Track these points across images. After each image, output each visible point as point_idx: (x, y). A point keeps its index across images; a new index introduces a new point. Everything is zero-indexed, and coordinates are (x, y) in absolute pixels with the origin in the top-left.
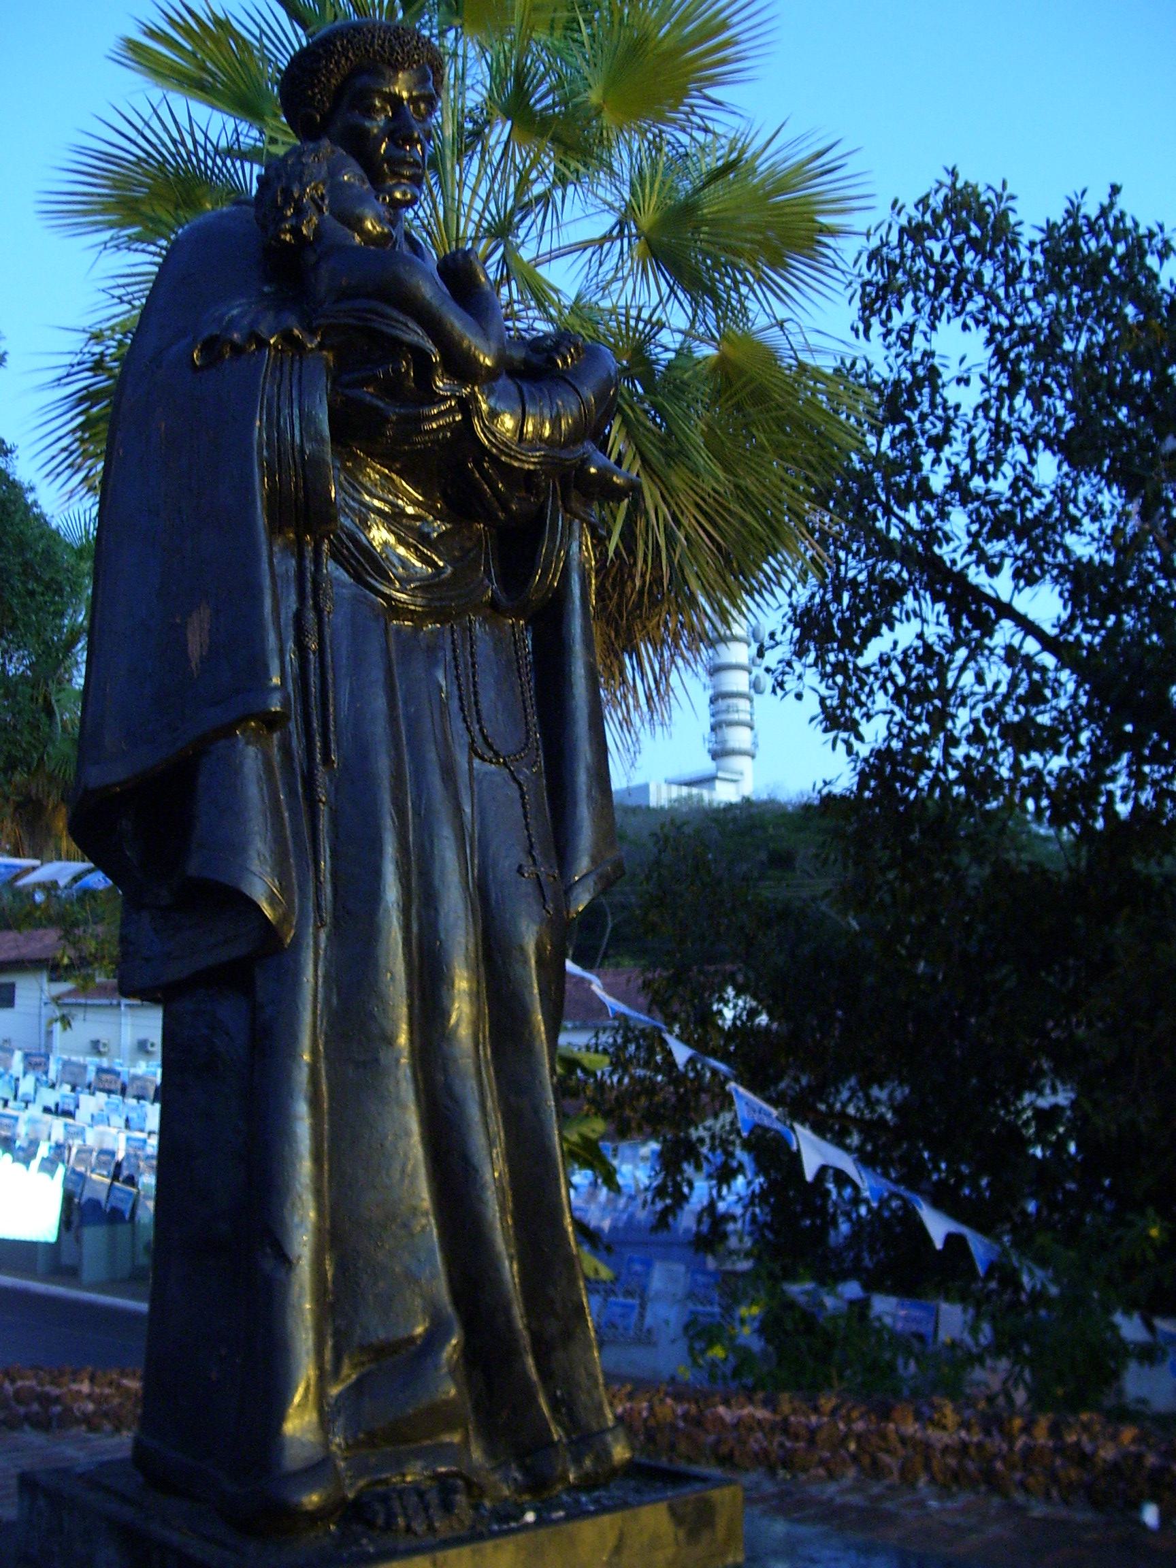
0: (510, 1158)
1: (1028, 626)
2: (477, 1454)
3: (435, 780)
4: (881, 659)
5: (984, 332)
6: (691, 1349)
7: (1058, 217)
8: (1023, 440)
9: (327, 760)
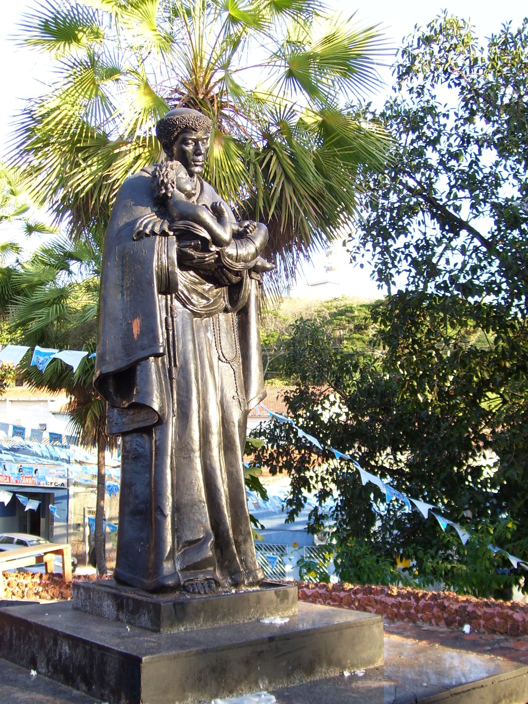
0: (229, 486)
1: (474, 233)
2: (218, 574)
3: (207, 370)
4: (405, 245)
5: (458, 89)
6: (300, 572)
7: (498, 33)
8: (477, 142)
9: (175, 365)
